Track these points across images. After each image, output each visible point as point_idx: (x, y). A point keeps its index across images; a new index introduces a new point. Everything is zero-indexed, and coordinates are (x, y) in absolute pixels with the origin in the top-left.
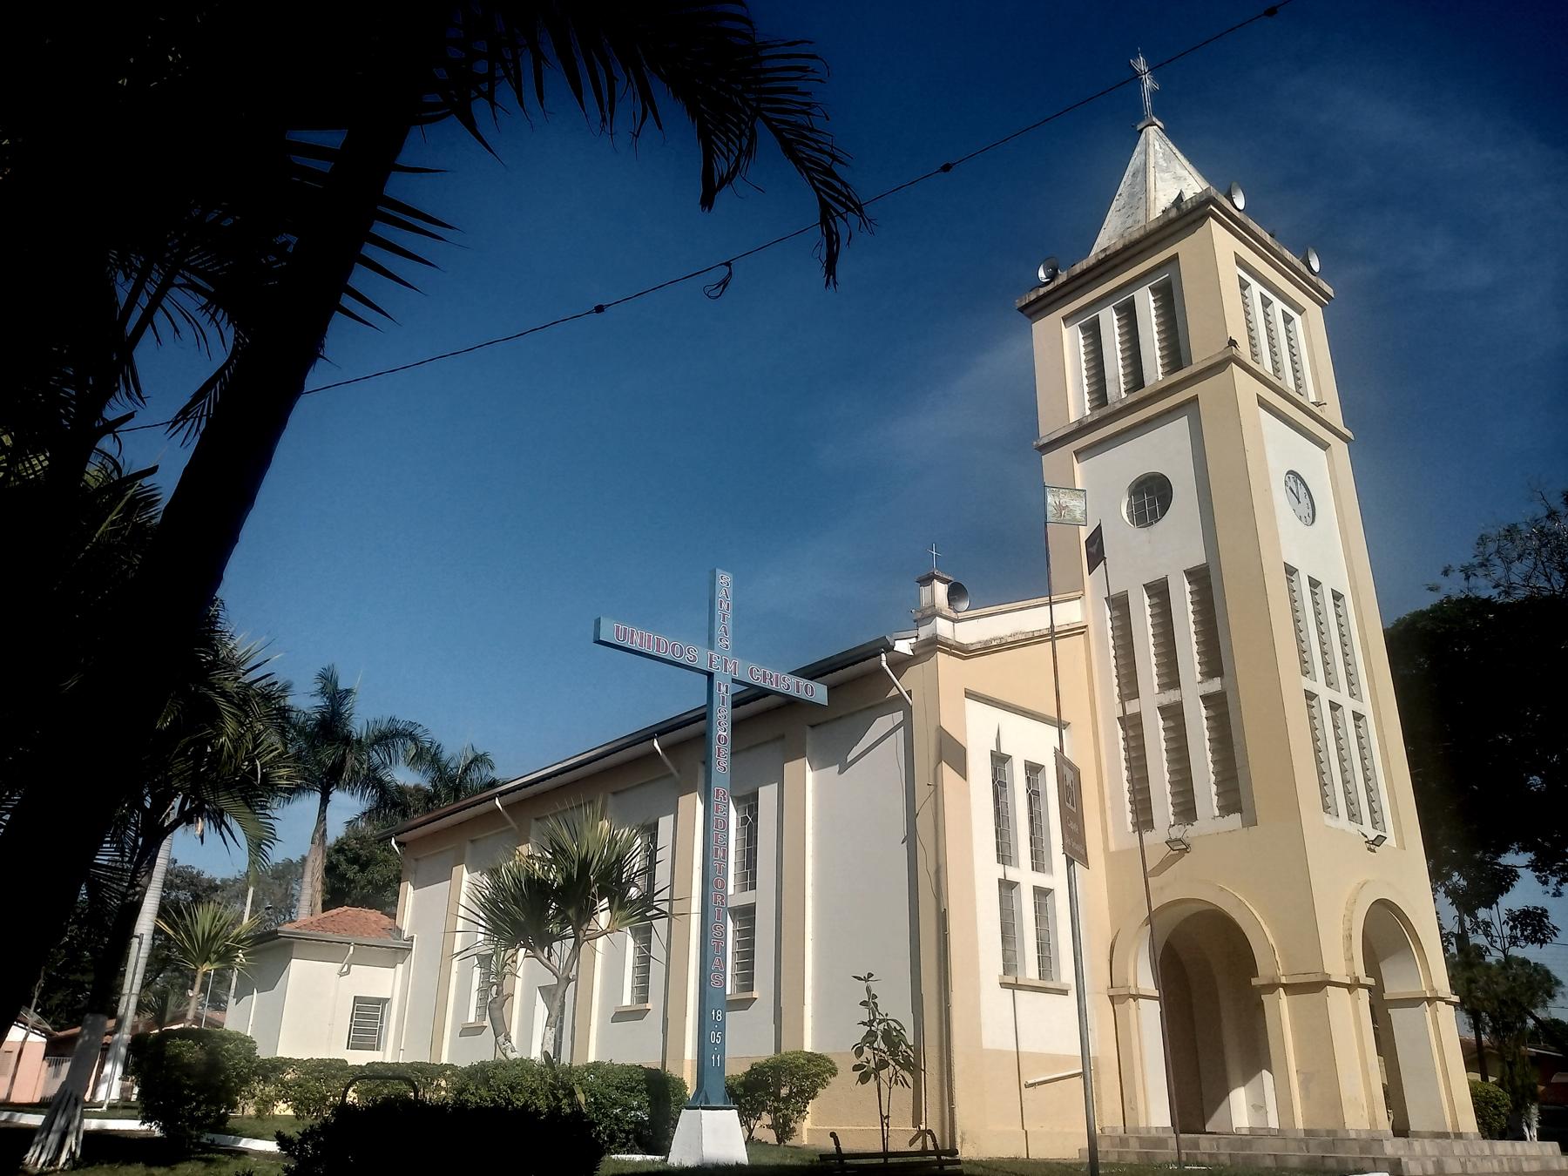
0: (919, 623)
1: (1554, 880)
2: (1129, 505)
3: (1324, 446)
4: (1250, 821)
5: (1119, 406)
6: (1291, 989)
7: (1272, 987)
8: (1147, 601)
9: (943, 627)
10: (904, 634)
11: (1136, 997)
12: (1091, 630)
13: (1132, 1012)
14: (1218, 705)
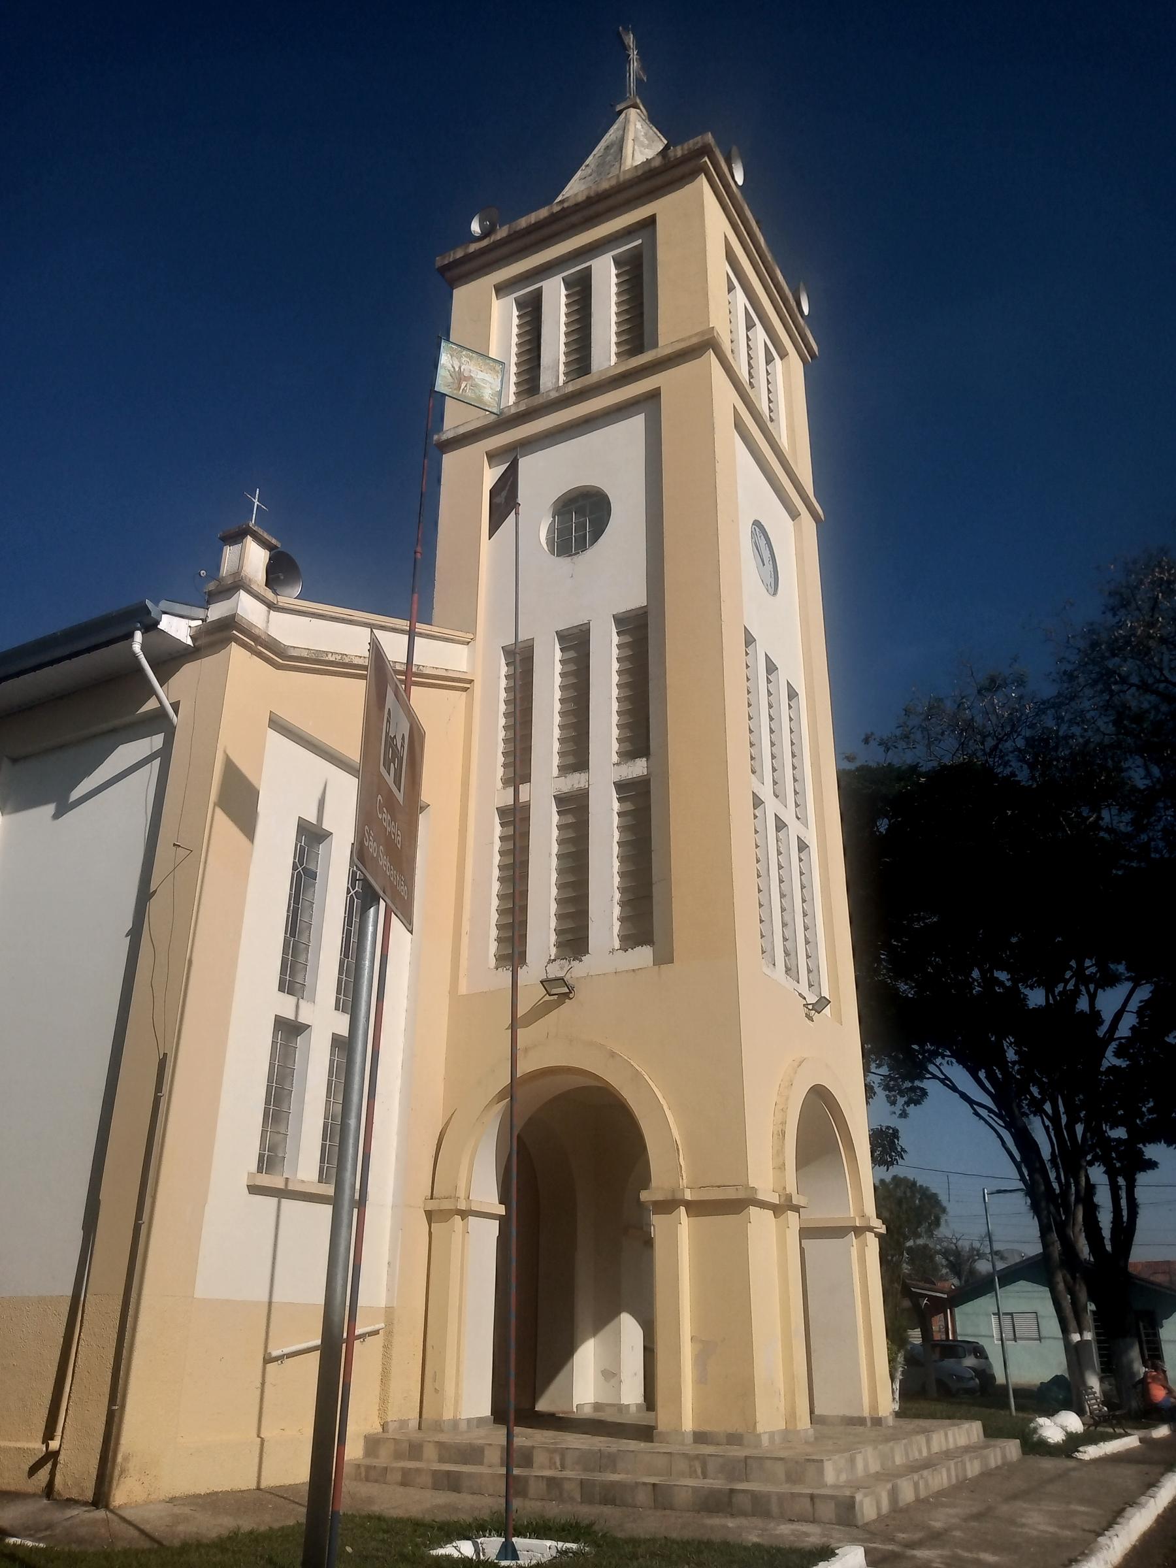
0: (211, 598)
1: (901, 1101)
2: (550, 530)
3: (794, 515)
4: (664, 958)
5: (554, 395)
6: (697, 1208)
7: (668, 1206)
8: (558, 655)
9: (248, 608)
10: (178, 608)
11: (464, 1214)
12: (477, 687)
13: (457, 1238)
14: (639, 800)
